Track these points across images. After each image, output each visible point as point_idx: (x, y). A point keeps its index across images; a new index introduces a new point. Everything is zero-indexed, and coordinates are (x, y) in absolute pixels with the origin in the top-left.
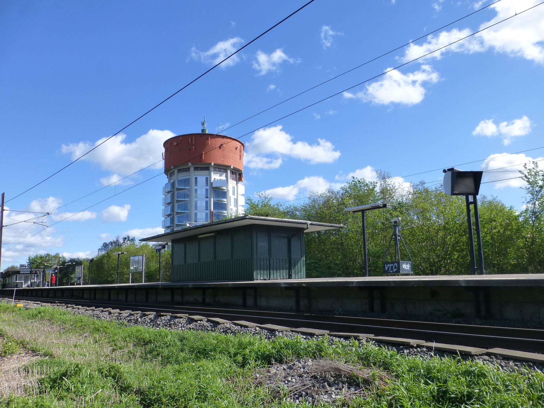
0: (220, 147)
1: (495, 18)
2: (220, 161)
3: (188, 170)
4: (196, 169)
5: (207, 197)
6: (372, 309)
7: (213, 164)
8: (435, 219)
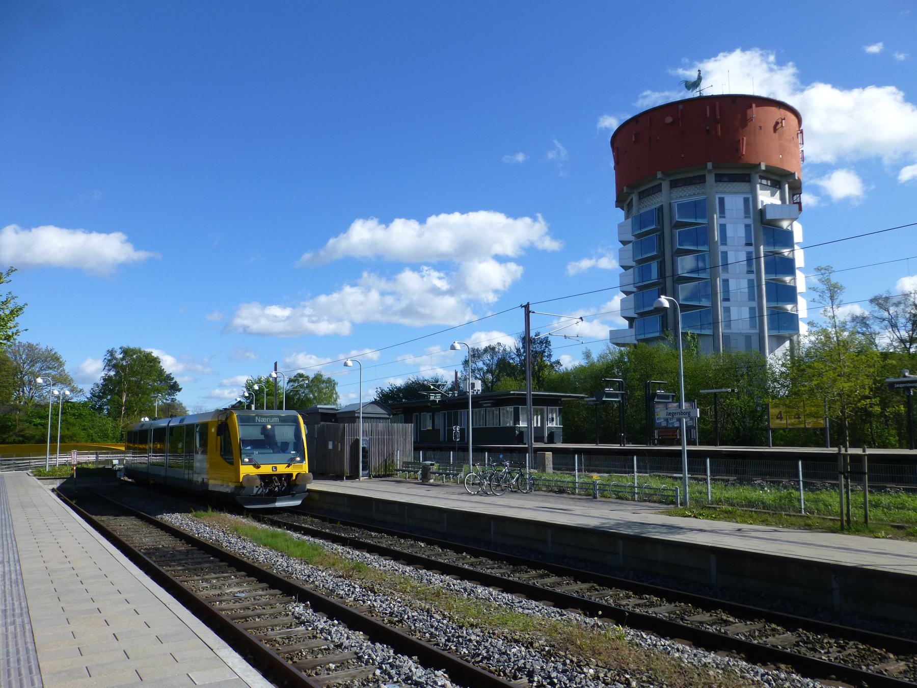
0: (775, 130)
1: (103, 236)
2: (777, 160)
3: (658, 189)
4: (719, 178)
5: (750, 244)
6: (681, 478)
7: (763, 167)
8: (610, 357)
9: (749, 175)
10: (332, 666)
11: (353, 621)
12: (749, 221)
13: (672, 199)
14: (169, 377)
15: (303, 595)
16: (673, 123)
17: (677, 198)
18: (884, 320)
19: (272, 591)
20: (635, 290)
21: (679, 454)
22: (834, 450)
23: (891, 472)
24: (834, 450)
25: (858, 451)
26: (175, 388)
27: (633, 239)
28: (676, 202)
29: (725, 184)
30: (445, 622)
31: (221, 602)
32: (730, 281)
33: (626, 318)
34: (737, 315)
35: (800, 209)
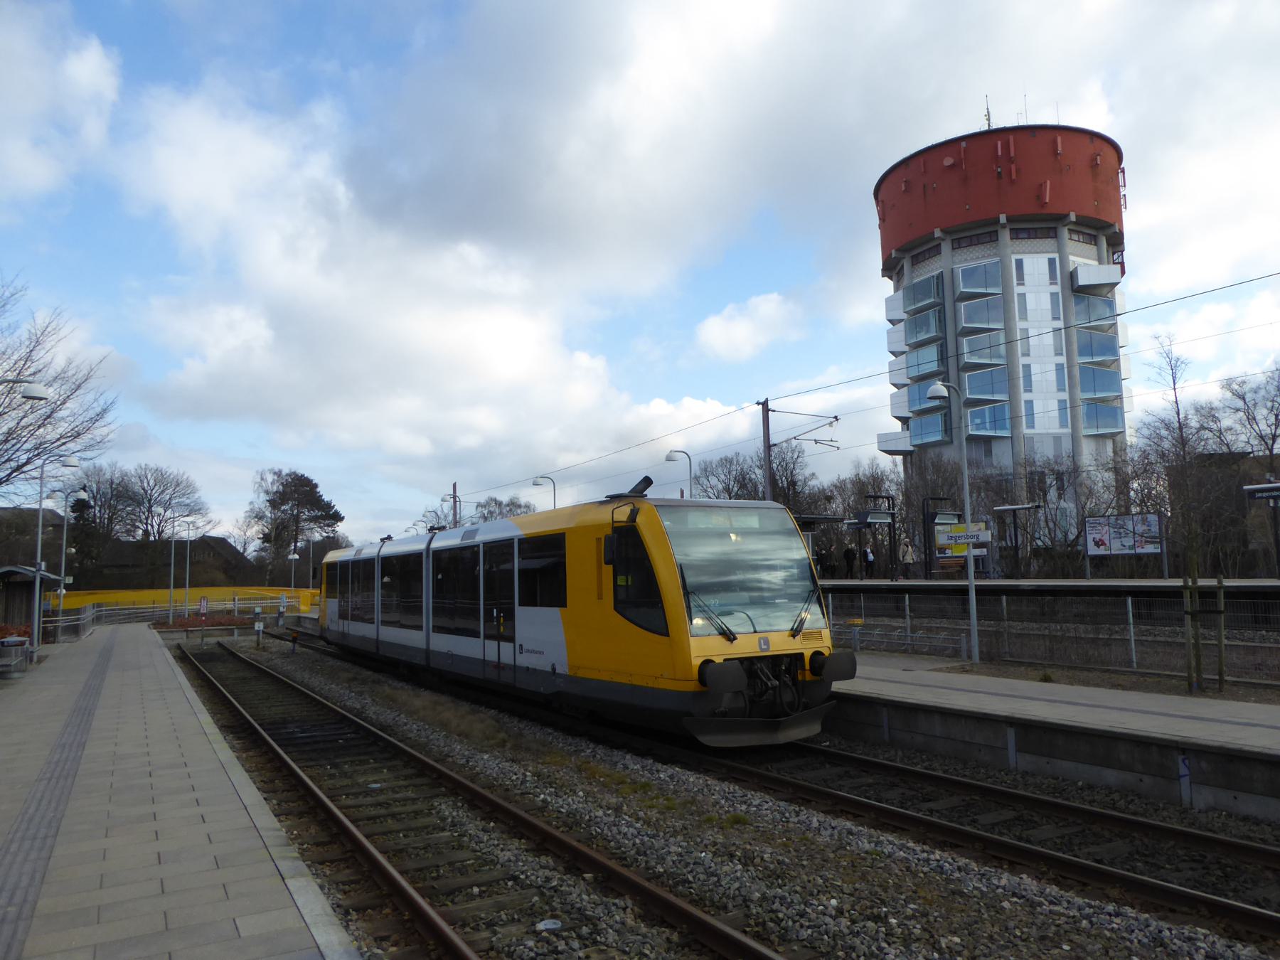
3: (936, 250)
4: (1016, 234)
9: (1055, 229)
10: (476, 890)
11: (518, 827)
12: (1057, 288)
13: (957, 264)
14: (329, 506)
15: (456, 789)
16: (952, 166)
17: (960, 262)
18: (1238, 410)
19: (418, 781)
20: (908, 381)
21: (964, 591)
22: (1178, 582)
23: (1258, 607)
24: (1178, 582)
25: (1212, 582)
26: (338, 518)
27: (905, 316)
28: (959, 268)
29: (1024, 242)
30: (638, 825)
31: (347, 795)
32: (1035, 403)
33: (897, 418)
34: (1044, 412)
35: (1123, 273)
